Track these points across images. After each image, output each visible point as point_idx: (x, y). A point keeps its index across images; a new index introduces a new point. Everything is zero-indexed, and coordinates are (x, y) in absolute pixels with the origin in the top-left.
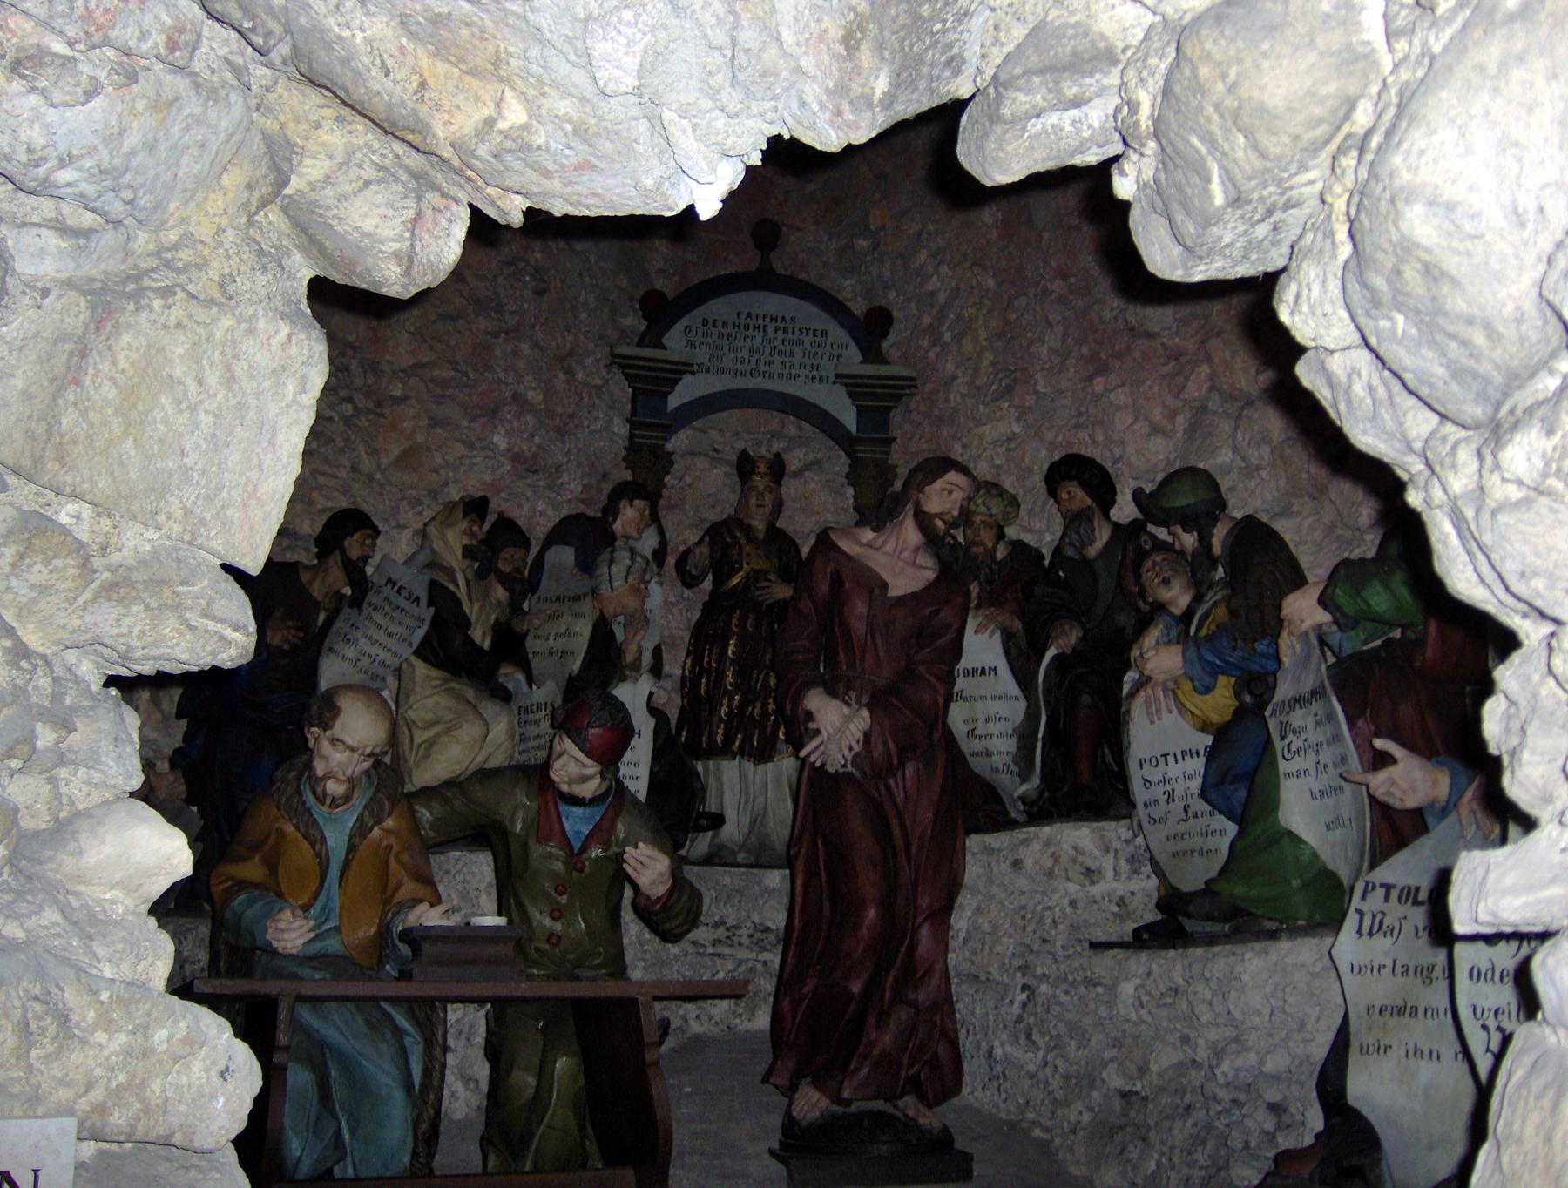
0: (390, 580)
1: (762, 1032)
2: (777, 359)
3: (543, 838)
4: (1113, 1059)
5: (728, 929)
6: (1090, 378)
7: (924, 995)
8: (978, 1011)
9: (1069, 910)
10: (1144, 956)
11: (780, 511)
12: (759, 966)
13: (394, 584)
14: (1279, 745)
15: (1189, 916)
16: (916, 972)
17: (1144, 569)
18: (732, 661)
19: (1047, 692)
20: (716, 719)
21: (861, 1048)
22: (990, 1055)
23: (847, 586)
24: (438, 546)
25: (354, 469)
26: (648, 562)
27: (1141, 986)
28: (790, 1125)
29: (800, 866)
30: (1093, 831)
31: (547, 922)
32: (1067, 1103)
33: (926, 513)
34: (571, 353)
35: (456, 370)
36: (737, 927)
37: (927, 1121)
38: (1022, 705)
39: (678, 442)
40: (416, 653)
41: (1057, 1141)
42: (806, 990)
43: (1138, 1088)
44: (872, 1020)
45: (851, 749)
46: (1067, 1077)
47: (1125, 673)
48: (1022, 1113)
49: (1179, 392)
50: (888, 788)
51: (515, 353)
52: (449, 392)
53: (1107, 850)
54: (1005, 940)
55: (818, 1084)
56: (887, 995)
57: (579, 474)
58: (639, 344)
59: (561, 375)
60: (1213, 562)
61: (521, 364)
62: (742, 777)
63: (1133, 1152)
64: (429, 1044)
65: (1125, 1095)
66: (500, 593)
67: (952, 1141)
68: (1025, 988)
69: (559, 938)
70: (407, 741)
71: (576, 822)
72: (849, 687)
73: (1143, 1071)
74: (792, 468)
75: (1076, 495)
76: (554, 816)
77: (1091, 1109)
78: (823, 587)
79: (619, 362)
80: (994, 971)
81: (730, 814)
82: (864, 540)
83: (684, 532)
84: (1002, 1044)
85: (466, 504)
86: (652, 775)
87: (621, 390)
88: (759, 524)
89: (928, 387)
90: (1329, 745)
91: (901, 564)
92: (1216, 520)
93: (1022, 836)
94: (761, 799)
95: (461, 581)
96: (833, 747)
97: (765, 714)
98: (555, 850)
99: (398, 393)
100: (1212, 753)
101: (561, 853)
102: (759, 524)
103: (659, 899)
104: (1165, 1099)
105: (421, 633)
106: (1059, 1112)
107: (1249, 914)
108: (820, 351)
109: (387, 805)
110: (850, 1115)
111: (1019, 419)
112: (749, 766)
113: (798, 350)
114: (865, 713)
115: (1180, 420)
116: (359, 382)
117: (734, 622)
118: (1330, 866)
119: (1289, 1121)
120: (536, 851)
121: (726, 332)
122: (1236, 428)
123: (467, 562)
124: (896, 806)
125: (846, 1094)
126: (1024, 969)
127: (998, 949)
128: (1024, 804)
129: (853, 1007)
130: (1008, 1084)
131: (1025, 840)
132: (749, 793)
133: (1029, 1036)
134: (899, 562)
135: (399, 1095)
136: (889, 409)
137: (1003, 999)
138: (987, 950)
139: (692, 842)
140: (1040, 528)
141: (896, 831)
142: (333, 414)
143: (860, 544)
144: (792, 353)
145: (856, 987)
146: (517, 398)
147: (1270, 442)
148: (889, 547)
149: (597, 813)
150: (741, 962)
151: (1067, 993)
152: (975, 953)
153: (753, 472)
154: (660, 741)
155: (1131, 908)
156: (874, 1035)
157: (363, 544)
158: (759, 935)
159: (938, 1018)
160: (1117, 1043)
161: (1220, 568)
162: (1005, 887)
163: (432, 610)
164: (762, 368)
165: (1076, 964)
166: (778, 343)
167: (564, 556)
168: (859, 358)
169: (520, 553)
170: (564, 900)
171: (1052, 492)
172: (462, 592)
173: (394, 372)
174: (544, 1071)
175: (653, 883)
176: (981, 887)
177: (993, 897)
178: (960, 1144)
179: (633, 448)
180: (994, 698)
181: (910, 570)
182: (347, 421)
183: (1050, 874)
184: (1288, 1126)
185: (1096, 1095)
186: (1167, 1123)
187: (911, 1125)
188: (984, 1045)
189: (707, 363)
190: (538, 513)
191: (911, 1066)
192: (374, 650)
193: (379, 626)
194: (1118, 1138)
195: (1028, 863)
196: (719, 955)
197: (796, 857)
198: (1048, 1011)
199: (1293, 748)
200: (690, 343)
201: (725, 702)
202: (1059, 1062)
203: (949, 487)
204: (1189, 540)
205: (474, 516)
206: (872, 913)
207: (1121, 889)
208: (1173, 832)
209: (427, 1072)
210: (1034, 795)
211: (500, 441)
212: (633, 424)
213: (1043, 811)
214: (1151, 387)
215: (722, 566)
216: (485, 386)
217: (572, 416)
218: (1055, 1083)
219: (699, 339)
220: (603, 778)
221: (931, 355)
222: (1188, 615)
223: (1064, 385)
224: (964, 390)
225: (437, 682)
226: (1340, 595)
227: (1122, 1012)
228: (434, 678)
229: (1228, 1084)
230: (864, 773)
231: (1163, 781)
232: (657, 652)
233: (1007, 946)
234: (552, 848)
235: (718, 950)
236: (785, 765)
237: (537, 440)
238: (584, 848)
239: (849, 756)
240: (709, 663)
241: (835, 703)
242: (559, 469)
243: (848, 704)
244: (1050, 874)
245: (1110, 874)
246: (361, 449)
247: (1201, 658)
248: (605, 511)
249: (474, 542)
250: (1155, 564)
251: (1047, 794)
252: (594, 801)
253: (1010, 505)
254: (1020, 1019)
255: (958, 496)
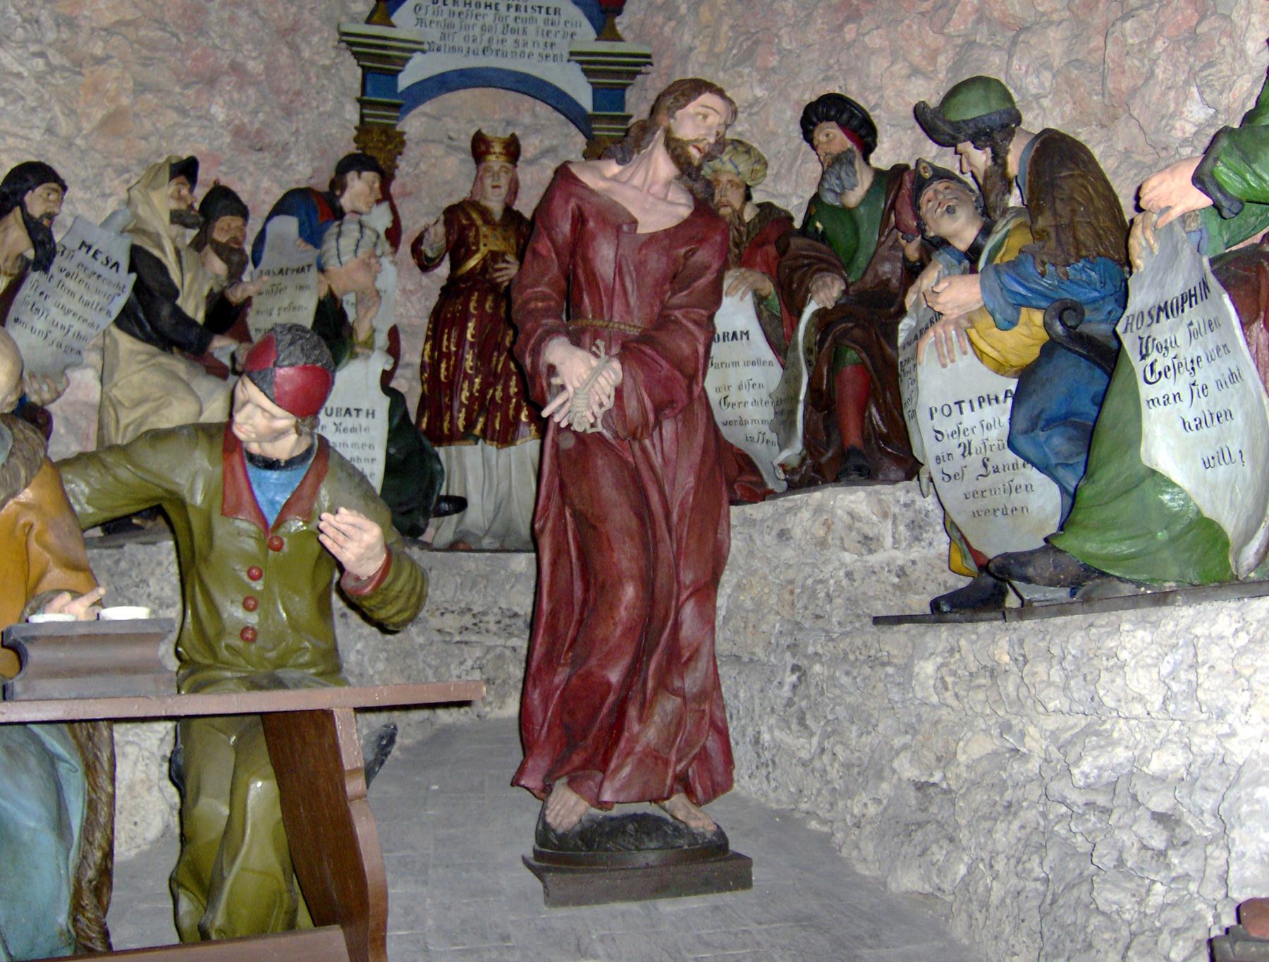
0: (83, 243)
1: (509, 719)
2: (510, 38)
3: (230, 511)
4: (905, 747)
5: (474, 616)
6: (841, 27)
7: (692, 681)
8: (742, 694)
9: (845, 582)
10: (944, 631)
11: (515, 193)
12: (508, 653)
13: (90, 248)
14: (1139, 366)
15: (1028, 580)
16: (680, 656)
17: (923, 200)
18: (472, 345)
19: (808, 351)
20: (456, 404)
21: (622, 744)
22: (757, 741)
23: (591, 224)
24: (142, 211)
25: (50, 131)
26: (378, 236)
27: (942, 665)
28: (544, 833)
29: (546, 542)
30: (869, 494)
31: (239, 613)
32: (849, 794)
33: (678, 140)
34: (294, 29)
35: (164, 30)
36: (484, 613)
37: (700, 824)
38: (776, 373)
39: (412, 125)
40: (119, 323)
41: (839, 836)
42: (557, 680)
43: (937, 777)
44: (633, 712)
45: (601, 405)
46: (847, 766)
47: (898, 323)
48: (796, 802)
49: (943, 27)
50: (644, 450)
51: (233, 19)
52: (158, 55)
53: (885, 515)
54: (771, 617)
55: (573, 784)
56: (650, 684)
57: (309, 156)
58: (369, 21)
59: (286, 50)
60: (1007, 184)
61: (240, 32)
62: (486, 461)
63: (938, 855)
64: (90, 769)
65: (920, 787)
66: (218, 266)
67: (726, 844)
68: (795, 668)
69: (255, 633)
70: (113, 423)
71: (273, 491)
72: (596, 335)
73: (946, 759)
74: (528, 155)
75: (833, 136)
76: (243, 485)
77: (878, 801)
78: (565, 227)
79: (350, 42)
80: (760, 653)
81: (474, 500)
82: (609, 174)
83: (422, 216)
84: (771, 729)
85: (172, 166)
86: (388, 456)
87: (352, 74)
88: (496, 206)
89: (665, 63)
90: (1210, 359)
91: (650, 199)
92: (1011, 134)
93: (788, 505)
94: (504, 485)
95: (169, 248)
96: (580, 403)
97: (507, 398)
98: (244, 525)
99: (98, 50)
100: (1018, 398)
101: (253, 528)
102: (496, 206)
103: (370, 578)
104: (979, 796)
105: (121, 302)
106: (841, 804)
107: (1103, 574)
108: (553, 29)
109: (23, 473)
110: (612, 819)
111: (761, 81)
112: (491, 449)
113: (531, 28)
114: (616, 365)
115: (942, 59)
116: (51, 36)
117: (472, 305)
118: (1207, 513)
119: (1186, 838)
120: (222, 529)
121: (457, 9)
122: (1010, 56)
123: (176, 229)
124: (652, 468)
125: (607, 796)
126: (793, 647)
127: (764, 627)
128: (785, 472)
129: (611, 699)
130: (778, 772)
131: (789, 510)
132: (491, 476)
133: (802, 721)
134: (647, 193)
135: (47, 840)
136: (623, 87)
137: (770, 681)
138: (750, 629)
139: (437, 529)
140: (791, 186)
141: (655, 498)
142: (21, 69)
143: (601, 178)
144: (524, 31)
145: (614, 676)
146: (236, 68)
147: (1050, 68)
148: (637, 181)
149: (294, 477)
150: (489, 649)
151: (847, 673)
152: (737, 632)
153: (488, 152)
154: (396, 421)
155: (913, 577)
156: (636, 728)
157: (47, 200)
158: (507, 621)
159: (707, 707)
160: (910, 729)
161: (1016, 191)
162: (769, 561)
163: (134, 276)
164: (494, 46)
165: (858, 642)
166: (511, 21)
167: (288, 226)
168: (592, 34)
169: (236, 222)
170: (258, 586)
171: (808, 136)
172: (170, 261)
173: (93, 30)
174: (236, 795)
175: (360, 558)
176: (741, 562)
177: (756, 571)
178: (736, 845)
179: (364, 129)
180: (746, 364)
181: (662, 207)
182: (40, 78)
183: (823, 543)
184: (1185, 843)
185: (885, 786)
186: (987, 824)
187: (680, 829)
188: (750, 731)
189: (438, 42)
190: (260, 188)
191: (679, 761)
192: (67, 321)
193: (72, 294)
194: (918, 836)
195: (797, 532)
196: (466, 643)
197: (542, 530)
198: (822, 693)
199: (1158, 368)
200: (420, 22)
201: (466, 385)
202: (839, 749)
203: (703, 110)
204: (981, 159)
205: (182, 178)
206: (629, 592)
207: (900, 557)
208: (971, 489)
209: (92, 806)
210: (795, 462)
211: (219, 111)
212: (363, 103)
213: (803, 479)
214: (909, 27)
215: (458, 248)
216: (198, 51)
217: (298, 93)
218: (834, 773)
219: (429, 17)
220: (299, 433)
221: (667, 29)
222: (973, 253)
223: (811, 37)
224: (702, 59)
225: (143, 357)
226: (1223, 172)
227: (919, 695)
228: (139, 353)
229: (1088, 787)
230: (616, 436)
231: (958, 432)
232: (394, 334)
233: (773, 624)
234: (244, 524)
235: (465, 637)
236: (527, 446)
237: (261, 116)
238: (280, 522)
239: (599, 413)
240: (448, 347)
241: (580, 353)
242: (286, 148)
243: (597, 356)
244: (823, 543)
245: (888, 541)
246: (57, 109)
247: (1003, 288)
248: (333, 184)
249: (184, 207)
250: (936, 192)
251: (809, 461)
252: (291, 463)
253: (758, 161)
254: (790, 703)
255: (714, 120)
